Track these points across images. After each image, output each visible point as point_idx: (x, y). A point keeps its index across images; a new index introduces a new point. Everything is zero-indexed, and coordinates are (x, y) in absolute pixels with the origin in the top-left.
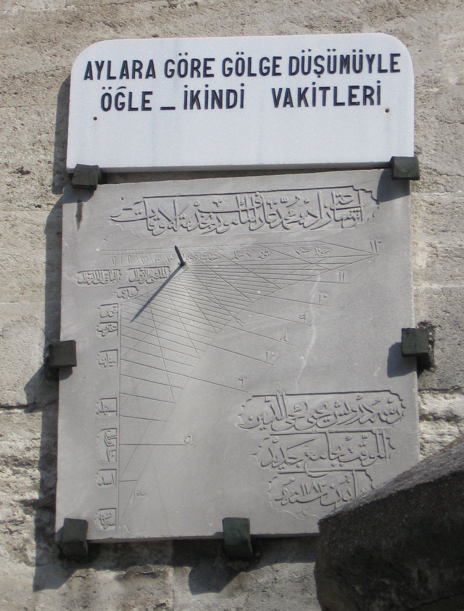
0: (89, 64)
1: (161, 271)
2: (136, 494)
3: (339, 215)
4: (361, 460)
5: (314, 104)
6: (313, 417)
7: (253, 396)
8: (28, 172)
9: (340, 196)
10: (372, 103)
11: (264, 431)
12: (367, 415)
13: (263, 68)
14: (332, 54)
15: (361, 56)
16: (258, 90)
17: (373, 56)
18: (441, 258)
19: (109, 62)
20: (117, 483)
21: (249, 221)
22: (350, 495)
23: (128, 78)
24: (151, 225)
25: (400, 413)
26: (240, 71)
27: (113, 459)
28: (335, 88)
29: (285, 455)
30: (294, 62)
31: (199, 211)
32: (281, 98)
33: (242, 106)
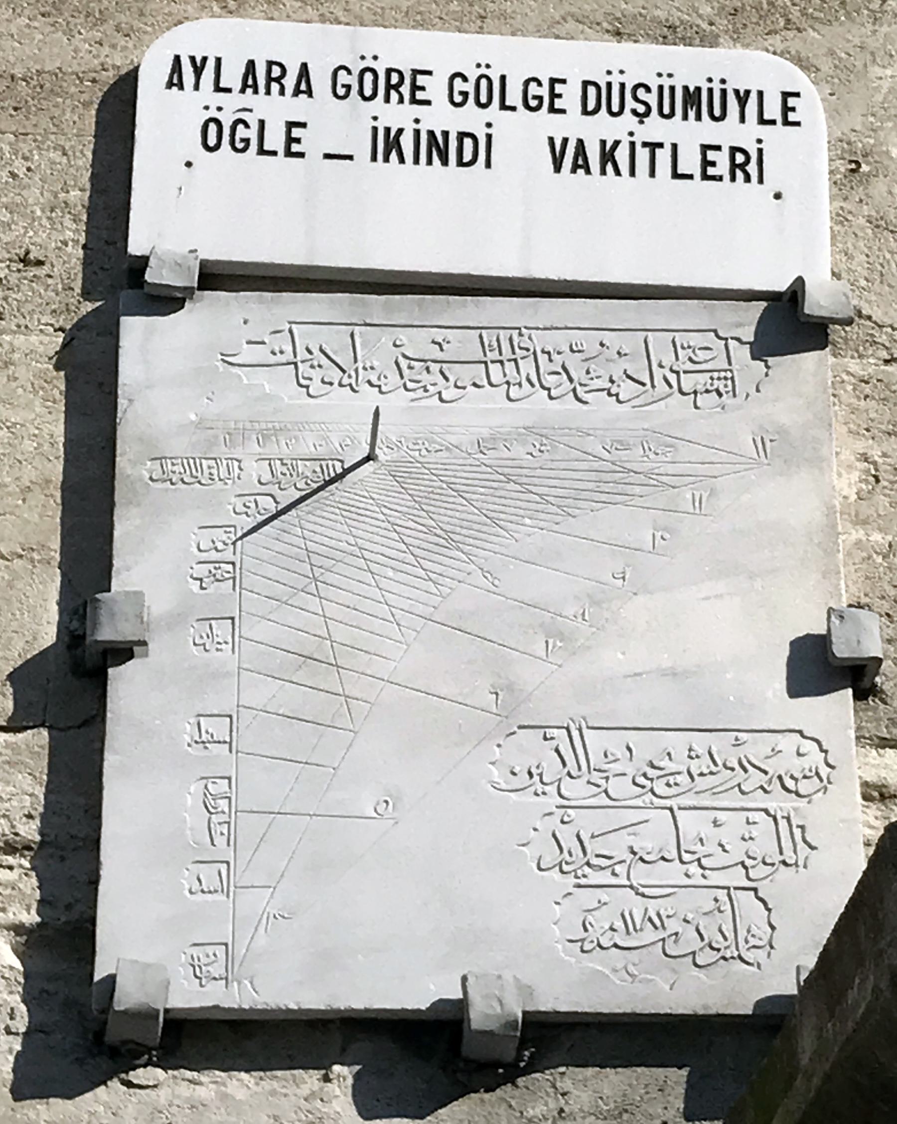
0: (177, 59)
1: (325, 468)
2: (272, 916)
3: (688, 382)
4: (746, 868)
5: (632, 173)
6: (645, 775)
7: (520, 727)
8: (40, 263)
9: (689, 347)
10: (748, 179)
11: (542, 798)
12: (757, 778)
13: (530, 96)
14: (667, 83)
15: (724, 92)
16: (521, 137)
17: (748, 92)
18: (886, 484)
19: (218, 60)
20: (232, 889)
21: (508, 383)
22: (725, 939)
23: (256, 92)
24: (306, 375)
25: (824, 776)
26: (483, 99)
27: (220, 841)
28: (675, 147)
29: (589, 851)
30: (592, 91)
31: (405, 356)
32: (568, 157)
33: (488, 165)
